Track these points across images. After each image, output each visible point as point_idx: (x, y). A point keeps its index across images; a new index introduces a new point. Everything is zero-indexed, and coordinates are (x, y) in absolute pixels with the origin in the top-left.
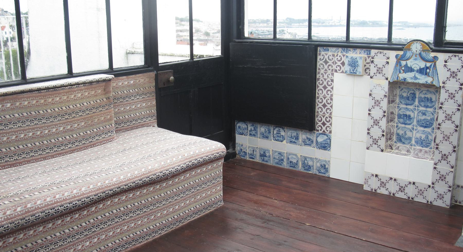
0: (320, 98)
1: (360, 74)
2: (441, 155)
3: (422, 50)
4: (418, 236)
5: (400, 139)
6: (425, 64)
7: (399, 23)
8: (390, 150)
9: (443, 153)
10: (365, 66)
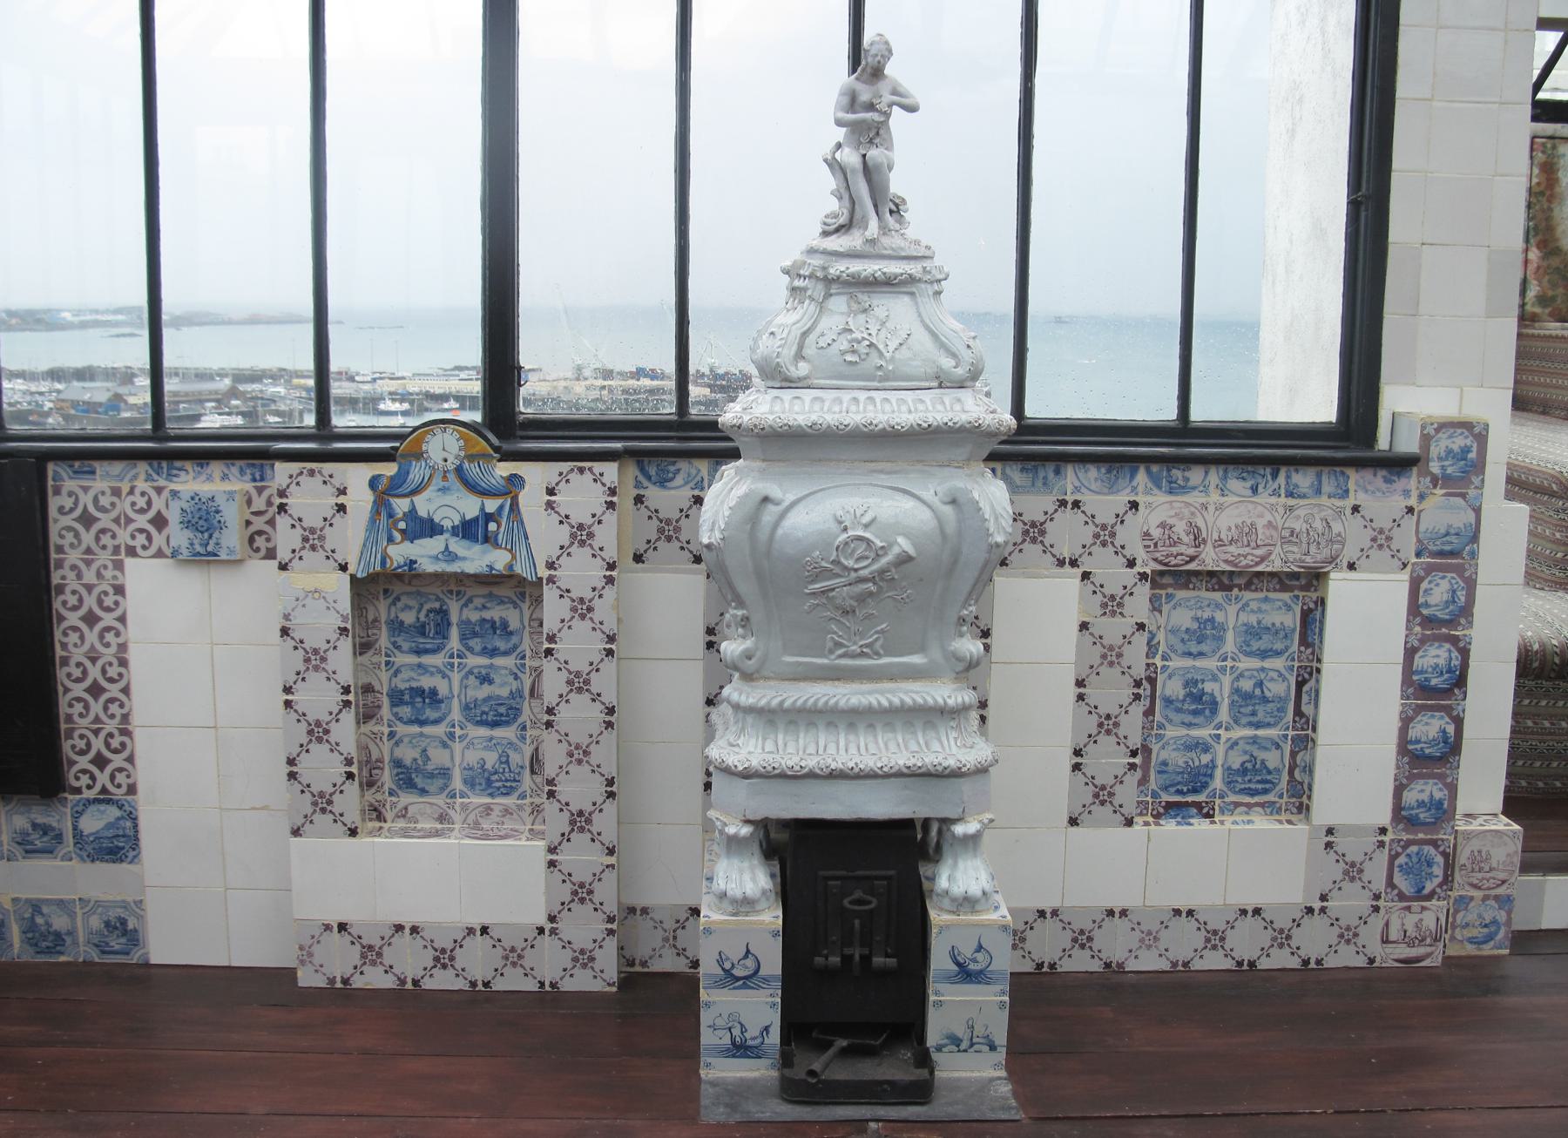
0: (73, 662)
1: (233, 558)
2: (566, 814)
4: (574, 1122)
5: (408, 779)
6: (480, 503)
7: (118, 311)
8: (378, 824)
9: (574, 808)
10: (248, 523)
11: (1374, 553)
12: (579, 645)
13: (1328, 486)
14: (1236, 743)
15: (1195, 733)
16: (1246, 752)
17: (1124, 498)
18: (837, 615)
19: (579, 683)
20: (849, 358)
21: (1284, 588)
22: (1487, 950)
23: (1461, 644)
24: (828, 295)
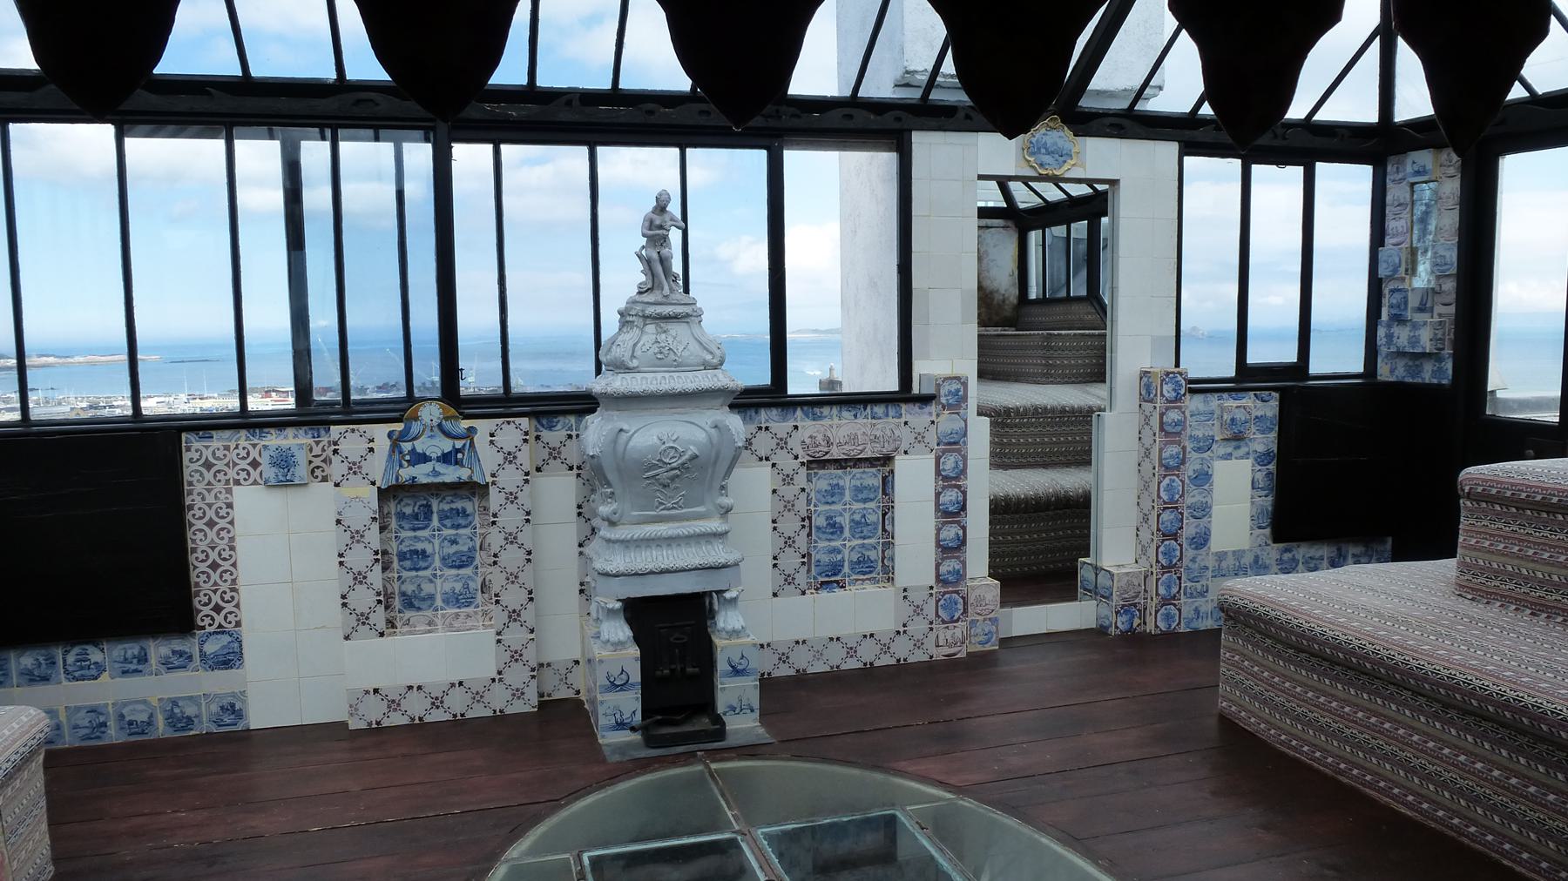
0: (199, 551)
3: (444, 418)
5: (409, 602)
10: (310, 462)
11: (916, 445)
12: (510, 518)
13: (892, 411)
14: (854, 548)
15: (833, 544)
16: (859, 553)
17: (791, 423)
18: (660, 488)
19: (511, 539)
20: (659, 356)
21: (873, 466)
22: (988, 647)
23: (963, 489)
24: (645, 325)
